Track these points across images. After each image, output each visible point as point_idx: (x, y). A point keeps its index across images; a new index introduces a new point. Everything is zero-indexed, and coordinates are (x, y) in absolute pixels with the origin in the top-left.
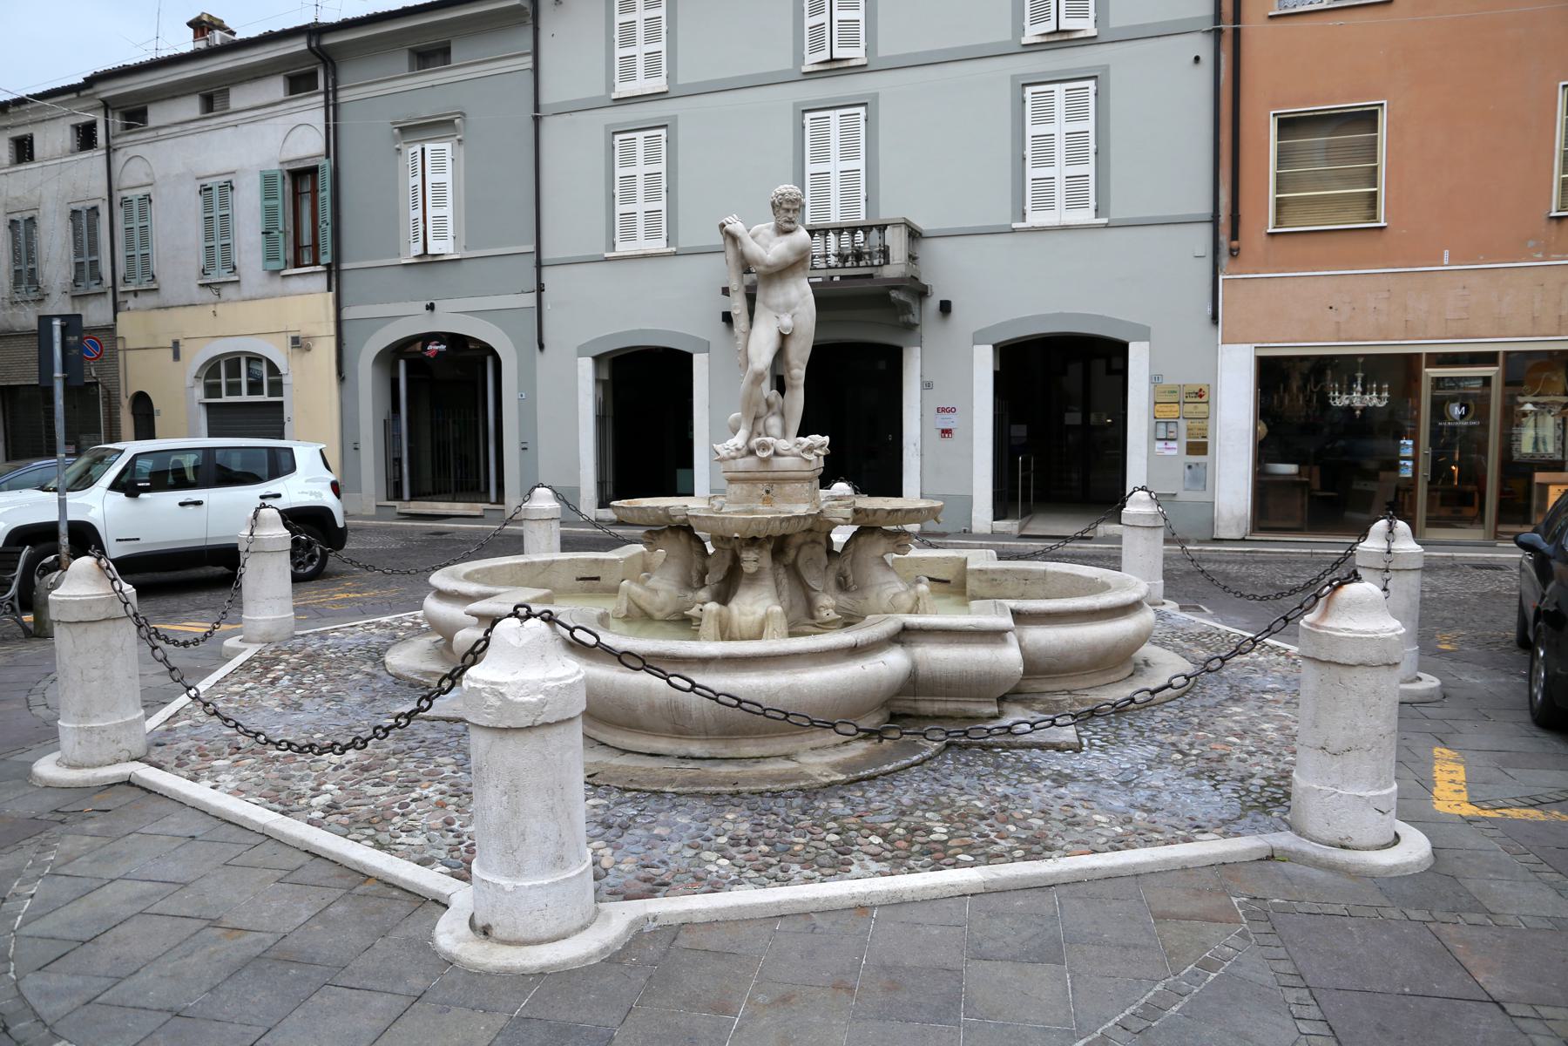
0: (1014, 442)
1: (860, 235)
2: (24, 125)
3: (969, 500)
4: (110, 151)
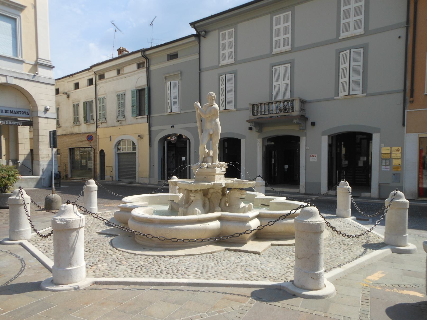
1: (286, 103)
3: (319, 184)
4: (96, 85)
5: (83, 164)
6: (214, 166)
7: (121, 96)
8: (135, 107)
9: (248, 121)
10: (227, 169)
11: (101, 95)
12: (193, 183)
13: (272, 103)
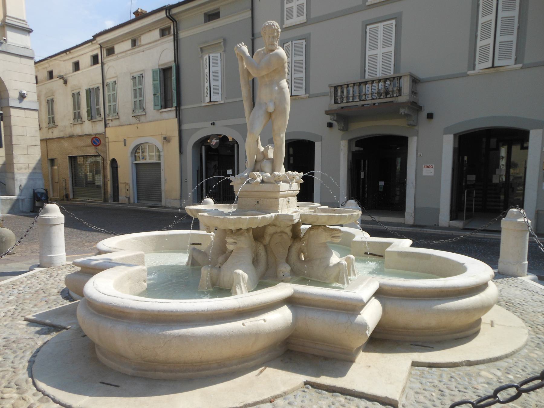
0: (468, 183)
1: (388, 83)
2: (77, 57)
3: (437, 211)
4: (103, 64)
5: (89, 180)
6: (276, 178)
7: (137, 80)
8: (159, 95)
9: (327, 113)
10: (301, 185)
11: (110, 78)
12: (233, 214)
13: (366, 83)
